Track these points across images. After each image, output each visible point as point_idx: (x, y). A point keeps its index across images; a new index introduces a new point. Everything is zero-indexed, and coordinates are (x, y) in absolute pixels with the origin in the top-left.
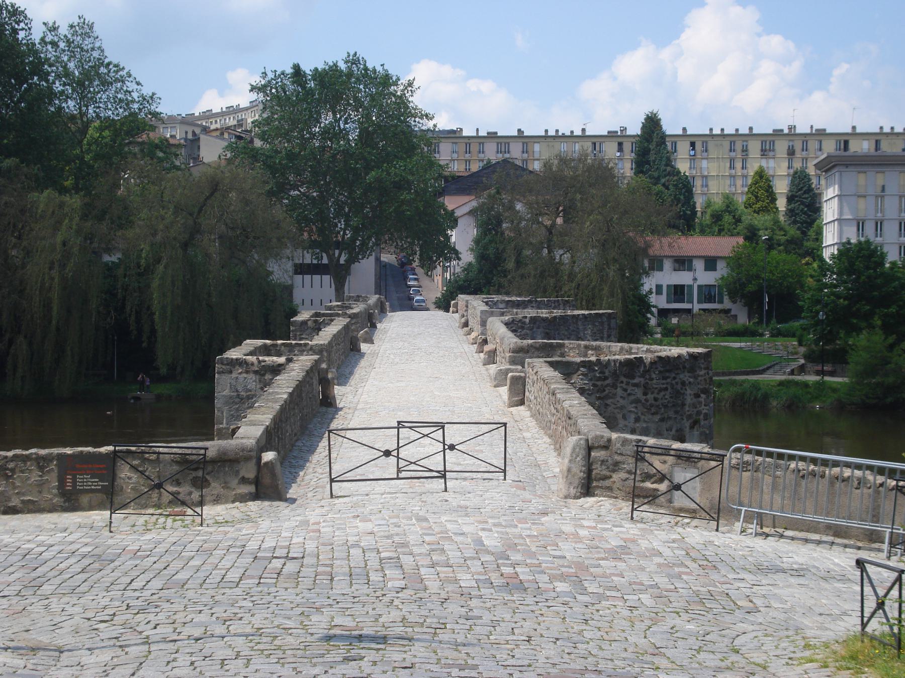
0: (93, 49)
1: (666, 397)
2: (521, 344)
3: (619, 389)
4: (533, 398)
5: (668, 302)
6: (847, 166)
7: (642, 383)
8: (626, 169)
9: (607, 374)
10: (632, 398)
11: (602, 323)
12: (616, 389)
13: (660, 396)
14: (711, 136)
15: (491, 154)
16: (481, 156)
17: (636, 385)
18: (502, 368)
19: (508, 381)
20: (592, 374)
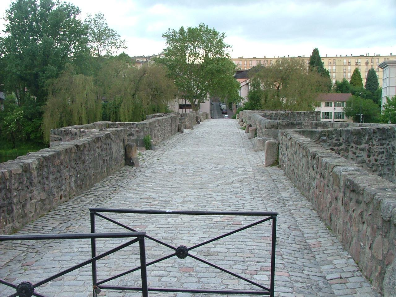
0: (103, 24)
1: (383, 158)
2: (273, 123)
3: (350, 153)
4: (286, 160)
5: (91, 232)
6: (392, 65)
7: (367, 148)
8: (307, 65)
9: (341, 141)
10: (360, 159)
11: (313, 117)
12: (348, 152)
13: (379, 158)
14: (337, 57)
15: (254, 64)
16: (251, 65)
17: (362, 150)
18: (260, 138)
19: (266, 147)
20: (330, 141)
